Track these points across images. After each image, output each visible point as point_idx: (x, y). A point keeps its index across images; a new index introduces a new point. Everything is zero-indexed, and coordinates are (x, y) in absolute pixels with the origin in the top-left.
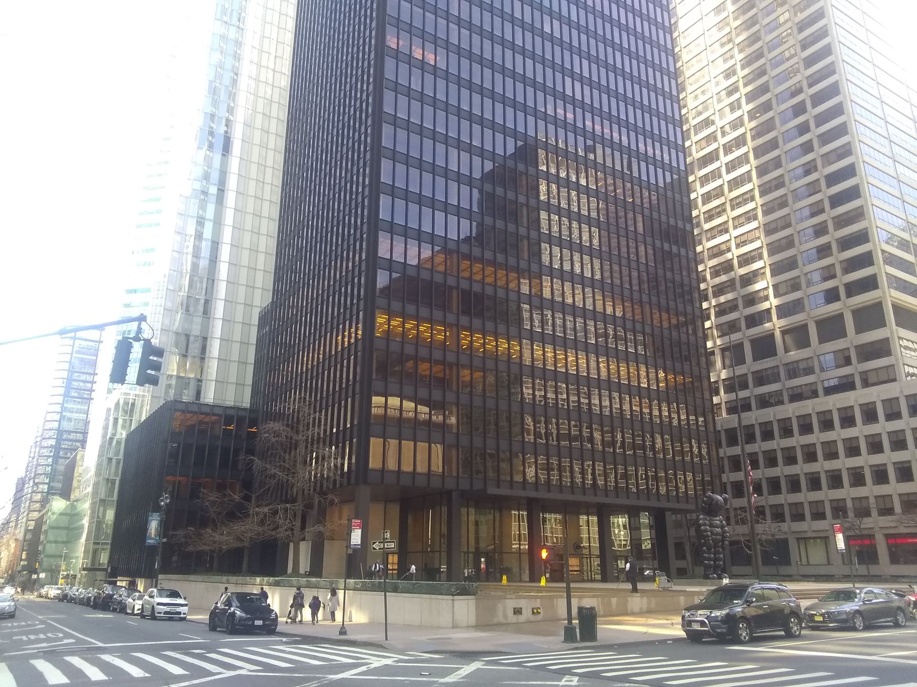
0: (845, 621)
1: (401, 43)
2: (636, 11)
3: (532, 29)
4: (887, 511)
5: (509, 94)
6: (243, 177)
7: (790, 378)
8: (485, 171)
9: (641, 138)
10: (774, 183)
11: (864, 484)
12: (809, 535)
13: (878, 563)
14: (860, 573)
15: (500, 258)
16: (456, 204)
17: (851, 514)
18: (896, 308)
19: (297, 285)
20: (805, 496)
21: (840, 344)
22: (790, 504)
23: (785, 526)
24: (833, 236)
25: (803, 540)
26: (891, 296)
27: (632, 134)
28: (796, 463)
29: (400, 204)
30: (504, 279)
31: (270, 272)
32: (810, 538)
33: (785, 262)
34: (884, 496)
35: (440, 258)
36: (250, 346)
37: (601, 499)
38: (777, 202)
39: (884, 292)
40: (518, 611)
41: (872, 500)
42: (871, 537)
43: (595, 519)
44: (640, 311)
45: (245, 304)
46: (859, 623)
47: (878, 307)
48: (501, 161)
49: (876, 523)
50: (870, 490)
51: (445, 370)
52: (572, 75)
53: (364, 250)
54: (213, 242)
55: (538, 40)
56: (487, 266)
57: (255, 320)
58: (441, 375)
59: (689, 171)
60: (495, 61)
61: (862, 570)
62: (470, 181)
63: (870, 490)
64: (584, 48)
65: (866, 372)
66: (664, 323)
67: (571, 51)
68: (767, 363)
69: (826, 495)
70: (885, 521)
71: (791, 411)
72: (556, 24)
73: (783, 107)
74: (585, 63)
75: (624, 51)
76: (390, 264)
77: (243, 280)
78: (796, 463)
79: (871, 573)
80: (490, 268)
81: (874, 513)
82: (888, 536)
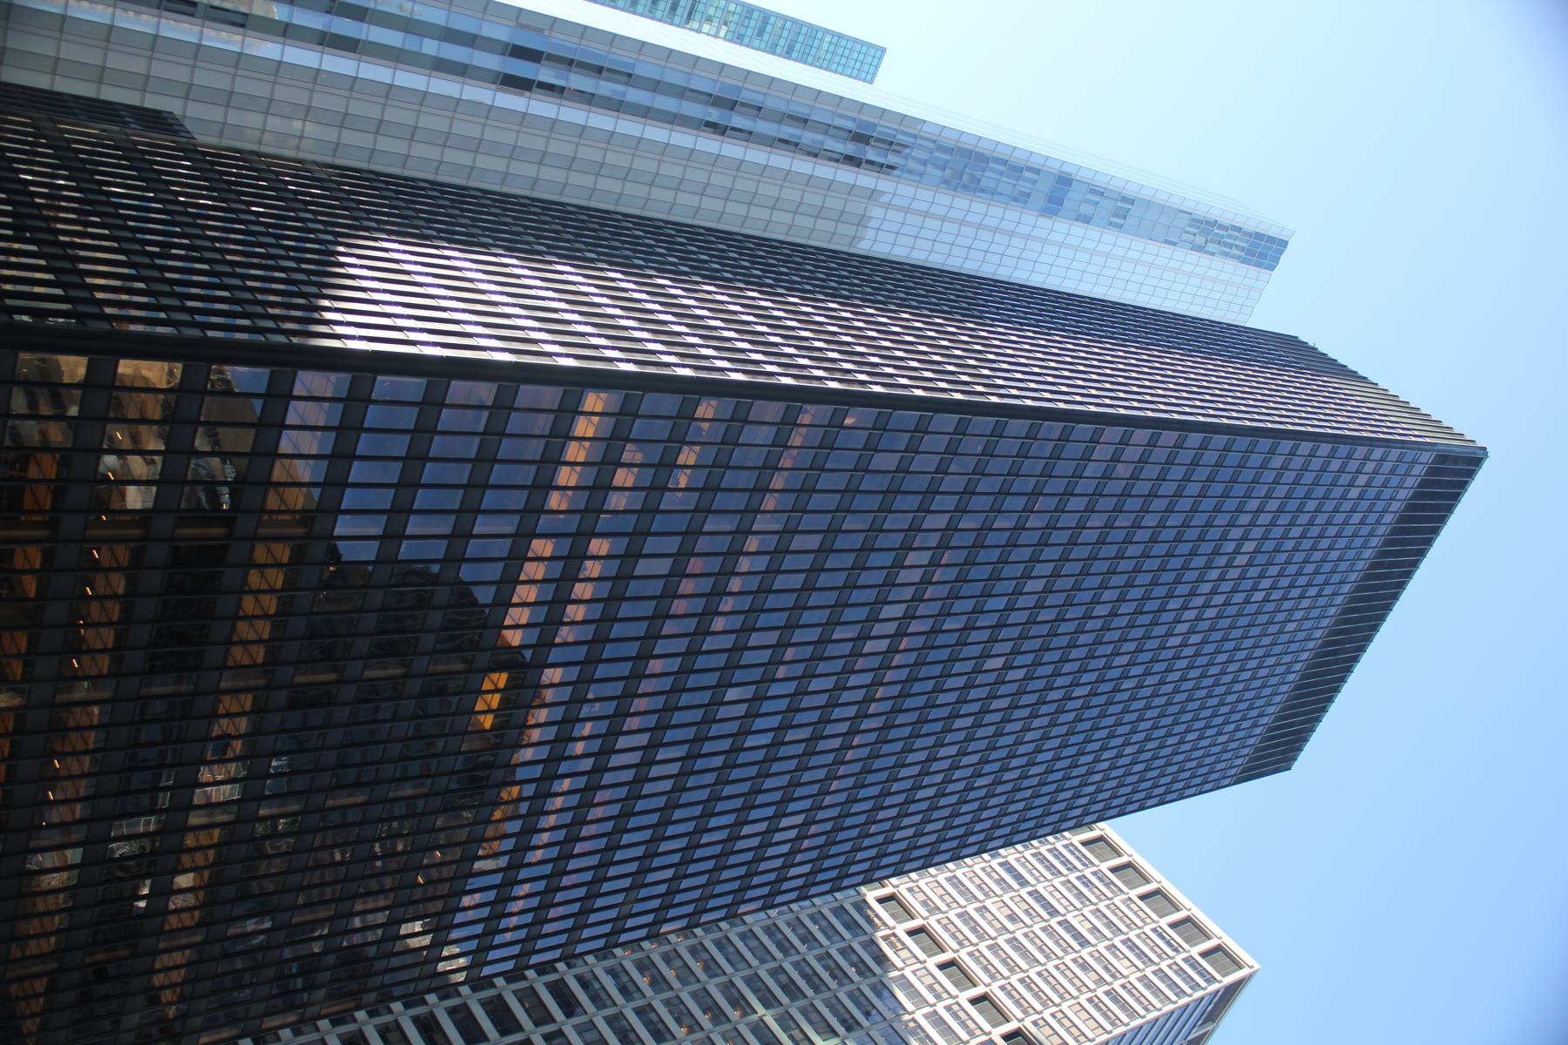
1: (705, 425)
2: (724, 859)
3: (732, 666)
6: (353, 83)
8: (474, 589)
9: (541, 885)
15: (299, 625)
16: (474, 532)
19: (234, 197)
27: (547, 869)
29: (408, 418)
30: (252, 636)
31: (561, 194)
35: (297, 499)
36: (406, 143)
44: (187, 923)
45: (190, 85)
51: (41, 511)
52: (654, 746)
53: (149, 329)
54: (466, 66)
55: (712, 679)
56: (279, 599)
57: (153, 102)
58: (28, 503)
59: (444, 992)
60: (855, 592)
62: (454, 559)
64: (700, 764)
66: (161, 976)
72: (741, 710)
74: (674, 768)
75: (561, 864)
76: (280, 395)
77: (244, 86)
80: (274, 603)
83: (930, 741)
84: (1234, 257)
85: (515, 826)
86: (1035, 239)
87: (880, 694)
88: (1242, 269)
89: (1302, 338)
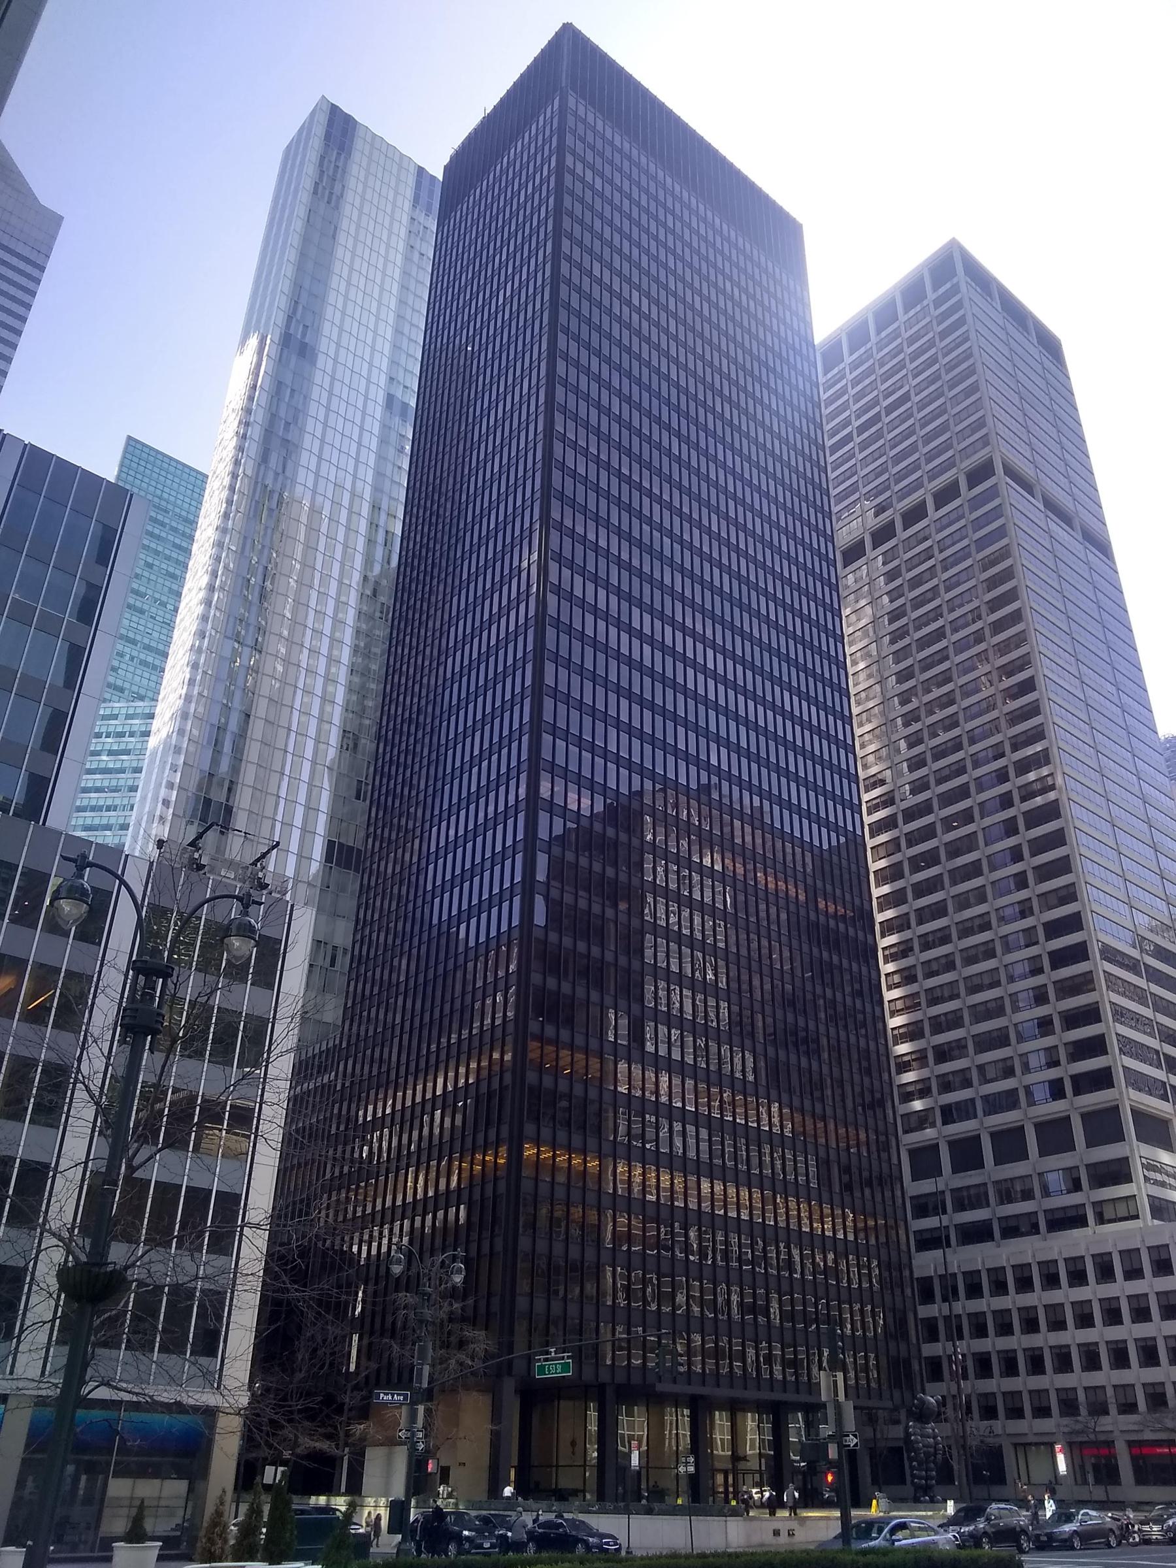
0: (1065, 1540)
4: (1129, 1408)
5: (624, 718)
7: (1002, 1203)
10: (977, 922)
11: (1043, 1372)
12: (1031, 1439)
13: (1119, 1484)
14: (1095, 1498)
17: (1083, 1411)
18: (1137, 1114)
20: (1024, 1382)
21: (1065, 1160)
22: (1004, 1394)
23: (998, 1425)
24: (1056, 1007)
25: (1023, 1446)
26: (1131, 1098)
28: (1093, 1326)
32: (1030, 1444)
33: (995, 1034)
34: (1123, 1386)
37: (778, 1396)
38: (982, 949)
39: (1121, 1093)
40: (776, 1533)
41: (1110, 1392)
42: (1110, 1444)
43: (686, 1412)
46: (1077, 1544)
47: (1114, 1111)
48: (584, 823)
49: (1115, 1424)
50: (1107, 1377)
61: (1099, 1493)
63: (1107, 1377)
65: (1101, 1202)
67: (832, 688)
68: (972, 1178)
69: (1051, 1381)
70: (1128, 1422)
71: (1056, 1250)
73: (988, 821)
78: (1093, 1326)
79: (1112, 1498)
81: (1113, 1409)
82: (1131, 1444)
83: (692, 405)
84: (345, 164)
85: (725, 785)
86: (334, 371)
87: (596, 345)
88: (356, 156)
89: (447, 160)
